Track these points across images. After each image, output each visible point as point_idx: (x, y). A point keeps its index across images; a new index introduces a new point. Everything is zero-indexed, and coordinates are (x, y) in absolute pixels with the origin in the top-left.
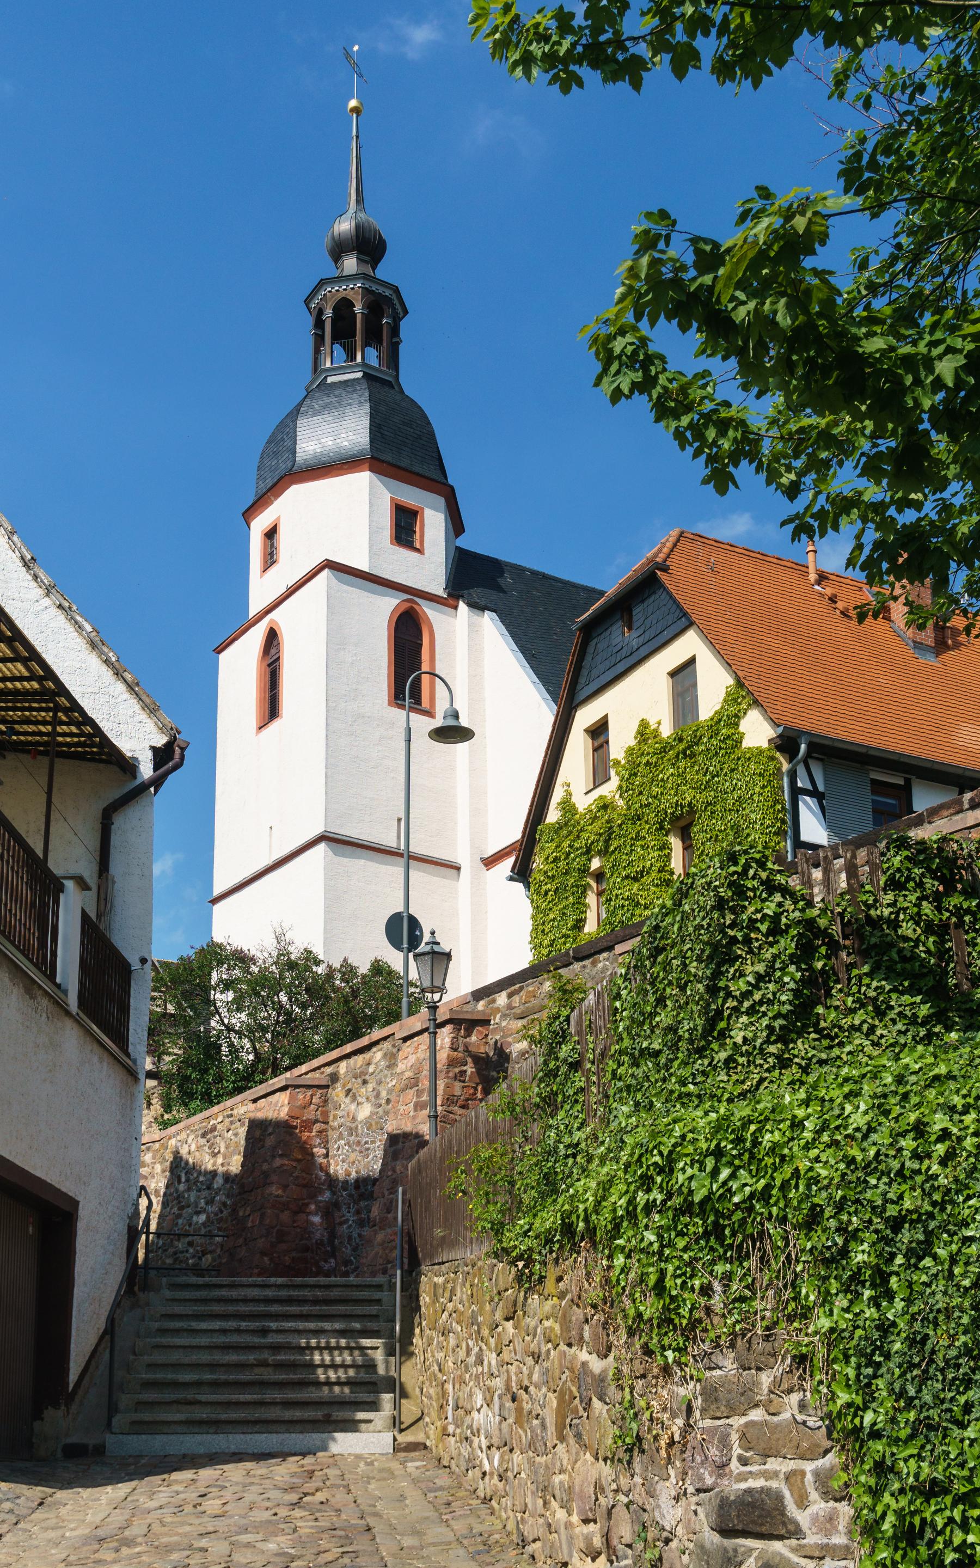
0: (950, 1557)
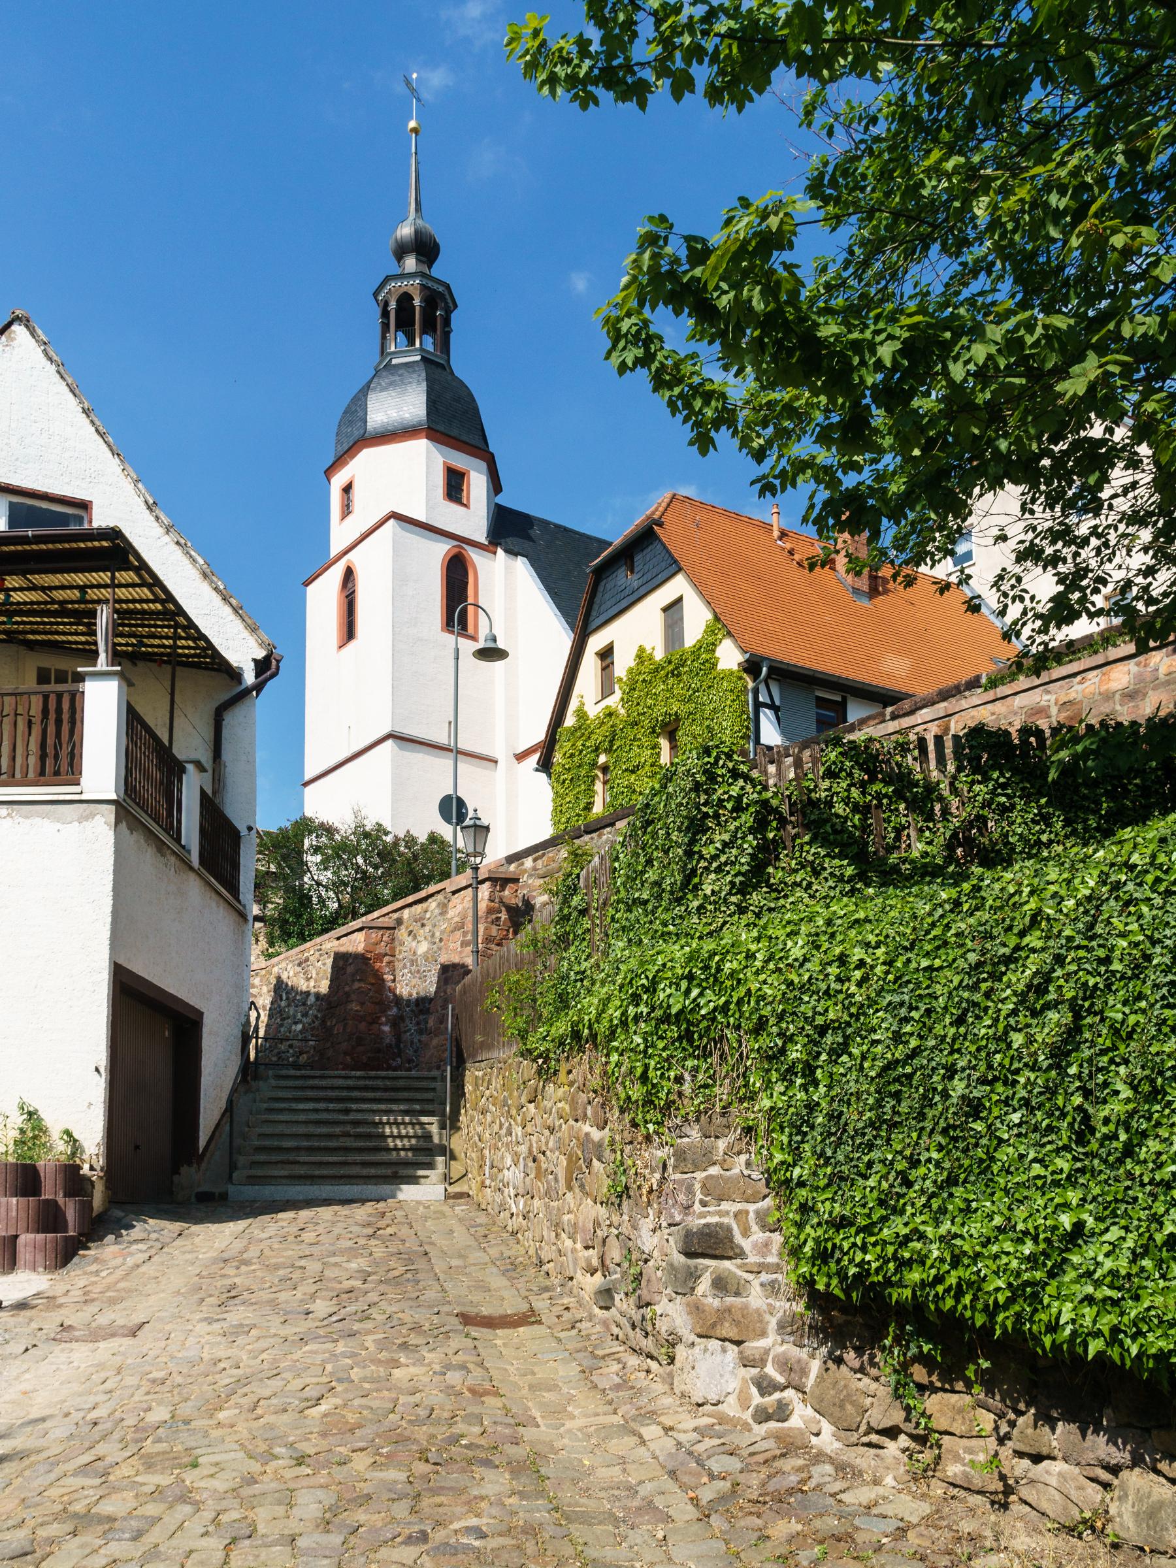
0: (852, 1271)
